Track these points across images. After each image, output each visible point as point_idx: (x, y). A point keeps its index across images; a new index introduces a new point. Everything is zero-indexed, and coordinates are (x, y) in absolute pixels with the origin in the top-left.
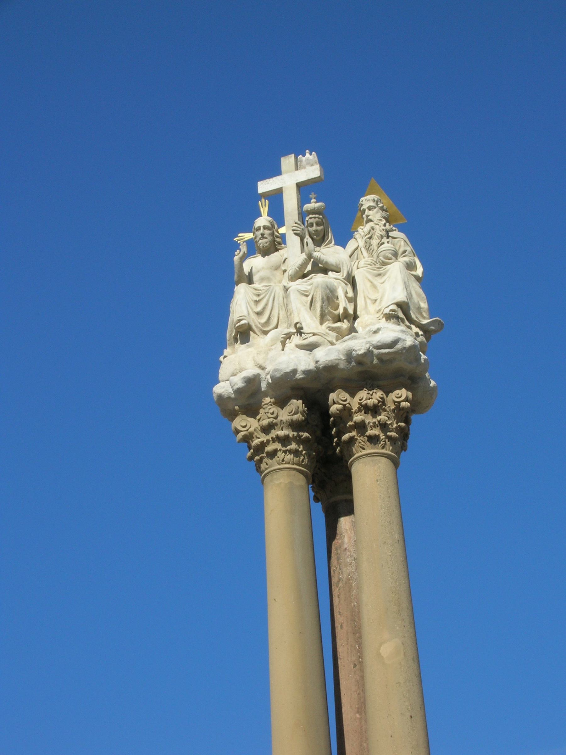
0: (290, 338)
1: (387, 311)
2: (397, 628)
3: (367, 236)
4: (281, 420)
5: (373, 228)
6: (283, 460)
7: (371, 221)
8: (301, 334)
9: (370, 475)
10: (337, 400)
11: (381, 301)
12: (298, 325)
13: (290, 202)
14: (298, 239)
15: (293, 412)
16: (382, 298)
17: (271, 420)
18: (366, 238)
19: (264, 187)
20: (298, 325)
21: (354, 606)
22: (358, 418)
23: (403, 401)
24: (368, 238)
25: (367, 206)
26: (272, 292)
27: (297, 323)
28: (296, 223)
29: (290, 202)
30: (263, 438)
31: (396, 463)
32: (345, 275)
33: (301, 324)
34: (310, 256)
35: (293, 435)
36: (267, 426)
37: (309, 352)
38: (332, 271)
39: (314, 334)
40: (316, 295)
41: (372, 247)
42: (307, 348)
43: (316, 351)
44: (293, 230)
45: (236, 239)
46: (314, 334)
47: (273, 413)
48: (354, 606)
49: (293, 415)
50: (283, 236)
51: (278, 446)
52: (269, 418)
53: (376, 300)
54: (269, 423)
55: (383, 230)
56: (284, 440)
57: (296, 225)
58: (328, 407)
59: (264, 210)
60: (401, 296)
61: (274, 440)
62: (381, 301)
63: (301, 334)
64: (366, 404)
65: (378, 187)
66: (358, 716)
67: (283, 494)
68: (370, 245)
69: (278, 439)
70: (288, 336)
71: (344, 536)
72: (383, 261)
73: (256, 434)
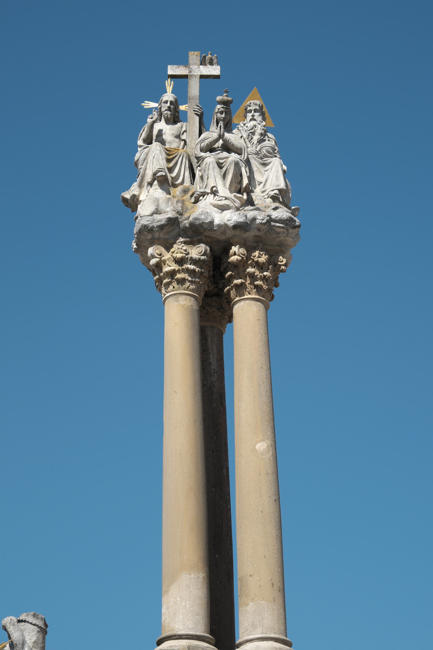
0: (204, 196)
1: (272, 193)
2: (269, 433)
3: (251, 131)
4: (191, 257)
5: (255, 126)
6: (188, 288)
7: (255, 120)
8: (215, 195)
9: (247, 314)
10: (236, 253)
11: (265, 184)
12: (214, 189)
13: (194, 88)
14: (197, 119)
15: (202, 253)
16: (266, 182)
17: (184, 255)
18: (249, 132)
19: (172, 70)
20: (214, 189)
21: (215, 407)
22: (250, 270)
23: (283, 265)
24: (251, 132)
25: (254, 108)
26: (181, 155)
27: (214, 187)
28: (197, 106)
29: (194, 88)
30: (174, 267)
31: (267, 308)
32: (245, 159)
33: (217, 188)
34: (221, 136)
35: (199, 270)
36: (180, 258)
37: (220, 211)
38: (235, 152)
39: (226, 199)
40: (229, 168)
41: (253, 140)
42: (220, 208)
43: (225, 212)
44: (194, 111)
45: (143, 104)
46: (226, 199)
47: (186, 250)
48: (215, 407)
49: (201, 255)
50: (185, 113)
51: (186, 276)
52: (182, 253)
53: (261, 183)
54: (182, 257)
55: (263, 129)
56: (191, 273)
57: (198, 108)
58: (228, 257)
59: (169, 89)
60: (282, 185)
61: (183, 271)
62: (265, 184)
63: (215, 195)
64: (258, 261)
65: (258, 95)
66: (213, 489)
67: (178, 313)
68: (252, 138)
69: (188, 271)
70: (203, 194)
71: (210, 353)
72: (265, 154)
73: (167, 262)
